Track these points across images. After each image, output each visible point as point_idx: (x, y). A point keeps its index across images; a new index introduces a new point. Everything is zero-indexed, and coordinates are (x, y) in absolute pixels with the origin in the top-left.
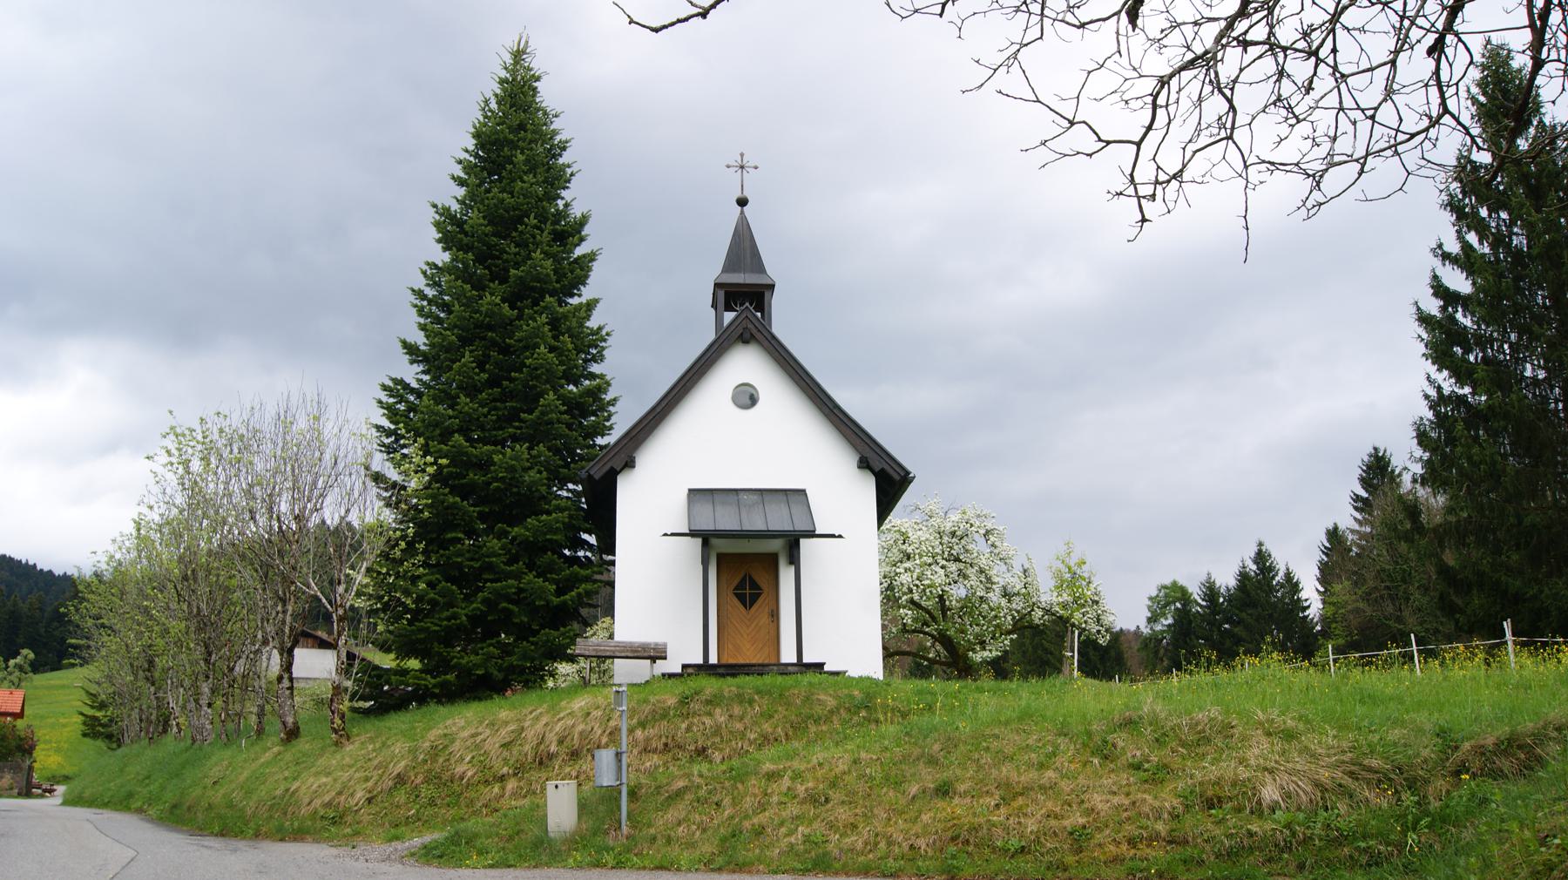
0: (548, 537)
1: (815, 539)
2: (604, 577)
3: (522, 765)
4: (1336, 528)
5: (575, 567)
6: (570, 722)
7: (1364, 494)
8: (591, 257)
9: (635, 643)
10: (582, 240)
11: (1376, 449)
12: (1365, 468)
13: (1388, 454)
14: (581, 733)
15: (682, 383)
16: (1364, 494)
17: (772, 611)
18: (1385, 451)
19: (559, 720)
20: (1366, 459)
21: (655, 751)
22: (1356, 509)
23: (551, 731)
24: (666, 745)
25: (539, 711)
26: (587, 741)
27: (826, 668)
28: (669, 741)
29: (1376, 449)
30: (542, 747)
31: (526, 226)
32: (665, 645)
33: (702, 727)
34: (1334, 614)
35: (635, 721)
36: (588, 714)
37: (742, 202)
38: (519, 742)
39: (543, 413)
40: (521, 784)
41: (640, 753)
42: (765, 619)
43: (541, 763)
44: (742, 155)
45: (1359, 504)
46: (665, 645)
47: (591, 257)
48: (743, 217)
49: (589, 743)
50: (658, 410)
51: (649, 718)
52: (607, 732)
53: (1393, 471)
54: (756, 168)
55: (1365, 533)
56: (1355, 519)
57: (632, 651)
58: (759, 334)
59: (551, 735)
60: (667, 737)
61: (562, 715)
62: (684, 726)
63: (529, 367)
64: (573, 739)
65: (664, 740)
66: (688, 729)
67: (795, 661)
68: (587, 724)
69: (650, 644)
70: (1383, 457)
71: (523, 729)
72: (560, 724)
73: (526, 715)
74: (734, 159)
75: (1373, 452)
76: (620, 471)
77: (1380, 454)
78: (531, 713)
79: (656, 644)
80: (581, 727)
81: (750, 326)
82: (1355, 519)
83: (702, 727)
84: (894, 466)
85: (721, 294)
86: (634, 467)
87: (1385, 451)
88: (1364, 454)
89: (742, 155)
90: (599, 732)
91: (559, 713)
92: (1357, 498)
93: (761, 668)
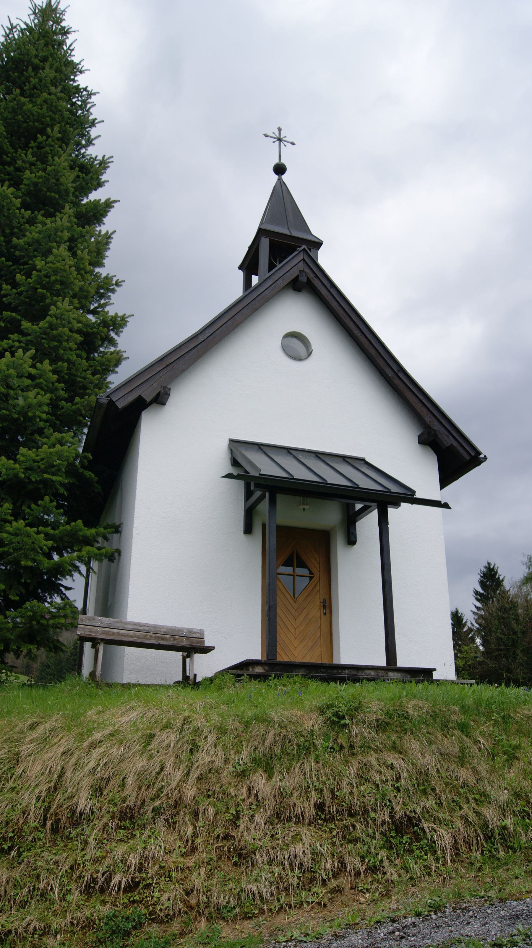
0: (46, 476)
1: (416, 506)
2: (108, 548)
3: (19, 832)
4: (457, 612)
5: (79, 522)
6: (116, 752)
7: (482, 591)
8: (109, 205)
9: (160, 627)
10: (100, 184)
11: (489, 564)
12: (482, 575)
13: (496, 567)
14: (139, 775)
15: (232, 313)
16: (482, 591)
17: (325, 601)
18: (494, 565)
19: (93, 746)
20: (483, 569)
21: (299, 819)
22: (477, 599)
23: (76, 767)
24: (320, 807)
25: (49, 725)
26: (153, 791)
27: (436, 676)
28: (328, 799)
29: (489, 564)
30: (60, 797)
31: (48, 137)
32: (202, 632)
33: (389, 774)
34: (464, 665)
35: (245, 755)
36: (152, 737)
37: (280, 169)
38: (11, 784)
39: (52, 327)
40: (16, 874)
41: (269, 822)
42: (316, 612)
43: (55, 830)
44: (280, 130)
45: (478, 597)
46: (202, 632)
47: (109, 205)
48: (280, 180)
49: (157, 796)
50: (201, 338)
51: (277, 751)
52: (194, 775)
53: (499, 578)
54: (293, 144)
55: (482, 616)
56: (475, 606)
57: (157, 638)
58: (316, 279)
59: (79, 775)
60: (320, 792)
61: (98, 736)
62: (353, 770)
63: (40, 271)
64: (123, 785)
65: (314, 796)
66: (362, 778)
67: (382, 662)
68: (150, 758)
69: (180, 630)
70: (493, 569)
71: (17, 758)
72: (96, 753)
73: (22, 732)
74: (273, 130)
75: (487, 565)
76: (151, 403)
77: (492, 567)
78: (33, 727)
79: (190, 631)
80: (140, 763)
81: (308, 271)
82: (475, 606)
83: (389, 774)
84: (464, 444)
85: (265, 243)
86: (163, 404)
87: (494, 565)
88: (482, 566)
89: (280, 130)
90: (179, 774)
91: (90, 732)
92: (477, 593)
93: (354, 672)
